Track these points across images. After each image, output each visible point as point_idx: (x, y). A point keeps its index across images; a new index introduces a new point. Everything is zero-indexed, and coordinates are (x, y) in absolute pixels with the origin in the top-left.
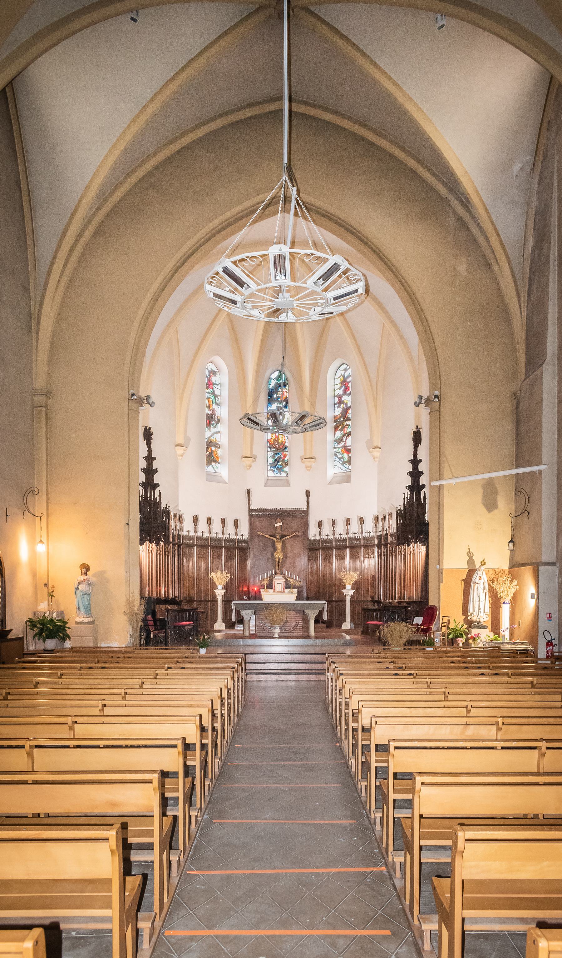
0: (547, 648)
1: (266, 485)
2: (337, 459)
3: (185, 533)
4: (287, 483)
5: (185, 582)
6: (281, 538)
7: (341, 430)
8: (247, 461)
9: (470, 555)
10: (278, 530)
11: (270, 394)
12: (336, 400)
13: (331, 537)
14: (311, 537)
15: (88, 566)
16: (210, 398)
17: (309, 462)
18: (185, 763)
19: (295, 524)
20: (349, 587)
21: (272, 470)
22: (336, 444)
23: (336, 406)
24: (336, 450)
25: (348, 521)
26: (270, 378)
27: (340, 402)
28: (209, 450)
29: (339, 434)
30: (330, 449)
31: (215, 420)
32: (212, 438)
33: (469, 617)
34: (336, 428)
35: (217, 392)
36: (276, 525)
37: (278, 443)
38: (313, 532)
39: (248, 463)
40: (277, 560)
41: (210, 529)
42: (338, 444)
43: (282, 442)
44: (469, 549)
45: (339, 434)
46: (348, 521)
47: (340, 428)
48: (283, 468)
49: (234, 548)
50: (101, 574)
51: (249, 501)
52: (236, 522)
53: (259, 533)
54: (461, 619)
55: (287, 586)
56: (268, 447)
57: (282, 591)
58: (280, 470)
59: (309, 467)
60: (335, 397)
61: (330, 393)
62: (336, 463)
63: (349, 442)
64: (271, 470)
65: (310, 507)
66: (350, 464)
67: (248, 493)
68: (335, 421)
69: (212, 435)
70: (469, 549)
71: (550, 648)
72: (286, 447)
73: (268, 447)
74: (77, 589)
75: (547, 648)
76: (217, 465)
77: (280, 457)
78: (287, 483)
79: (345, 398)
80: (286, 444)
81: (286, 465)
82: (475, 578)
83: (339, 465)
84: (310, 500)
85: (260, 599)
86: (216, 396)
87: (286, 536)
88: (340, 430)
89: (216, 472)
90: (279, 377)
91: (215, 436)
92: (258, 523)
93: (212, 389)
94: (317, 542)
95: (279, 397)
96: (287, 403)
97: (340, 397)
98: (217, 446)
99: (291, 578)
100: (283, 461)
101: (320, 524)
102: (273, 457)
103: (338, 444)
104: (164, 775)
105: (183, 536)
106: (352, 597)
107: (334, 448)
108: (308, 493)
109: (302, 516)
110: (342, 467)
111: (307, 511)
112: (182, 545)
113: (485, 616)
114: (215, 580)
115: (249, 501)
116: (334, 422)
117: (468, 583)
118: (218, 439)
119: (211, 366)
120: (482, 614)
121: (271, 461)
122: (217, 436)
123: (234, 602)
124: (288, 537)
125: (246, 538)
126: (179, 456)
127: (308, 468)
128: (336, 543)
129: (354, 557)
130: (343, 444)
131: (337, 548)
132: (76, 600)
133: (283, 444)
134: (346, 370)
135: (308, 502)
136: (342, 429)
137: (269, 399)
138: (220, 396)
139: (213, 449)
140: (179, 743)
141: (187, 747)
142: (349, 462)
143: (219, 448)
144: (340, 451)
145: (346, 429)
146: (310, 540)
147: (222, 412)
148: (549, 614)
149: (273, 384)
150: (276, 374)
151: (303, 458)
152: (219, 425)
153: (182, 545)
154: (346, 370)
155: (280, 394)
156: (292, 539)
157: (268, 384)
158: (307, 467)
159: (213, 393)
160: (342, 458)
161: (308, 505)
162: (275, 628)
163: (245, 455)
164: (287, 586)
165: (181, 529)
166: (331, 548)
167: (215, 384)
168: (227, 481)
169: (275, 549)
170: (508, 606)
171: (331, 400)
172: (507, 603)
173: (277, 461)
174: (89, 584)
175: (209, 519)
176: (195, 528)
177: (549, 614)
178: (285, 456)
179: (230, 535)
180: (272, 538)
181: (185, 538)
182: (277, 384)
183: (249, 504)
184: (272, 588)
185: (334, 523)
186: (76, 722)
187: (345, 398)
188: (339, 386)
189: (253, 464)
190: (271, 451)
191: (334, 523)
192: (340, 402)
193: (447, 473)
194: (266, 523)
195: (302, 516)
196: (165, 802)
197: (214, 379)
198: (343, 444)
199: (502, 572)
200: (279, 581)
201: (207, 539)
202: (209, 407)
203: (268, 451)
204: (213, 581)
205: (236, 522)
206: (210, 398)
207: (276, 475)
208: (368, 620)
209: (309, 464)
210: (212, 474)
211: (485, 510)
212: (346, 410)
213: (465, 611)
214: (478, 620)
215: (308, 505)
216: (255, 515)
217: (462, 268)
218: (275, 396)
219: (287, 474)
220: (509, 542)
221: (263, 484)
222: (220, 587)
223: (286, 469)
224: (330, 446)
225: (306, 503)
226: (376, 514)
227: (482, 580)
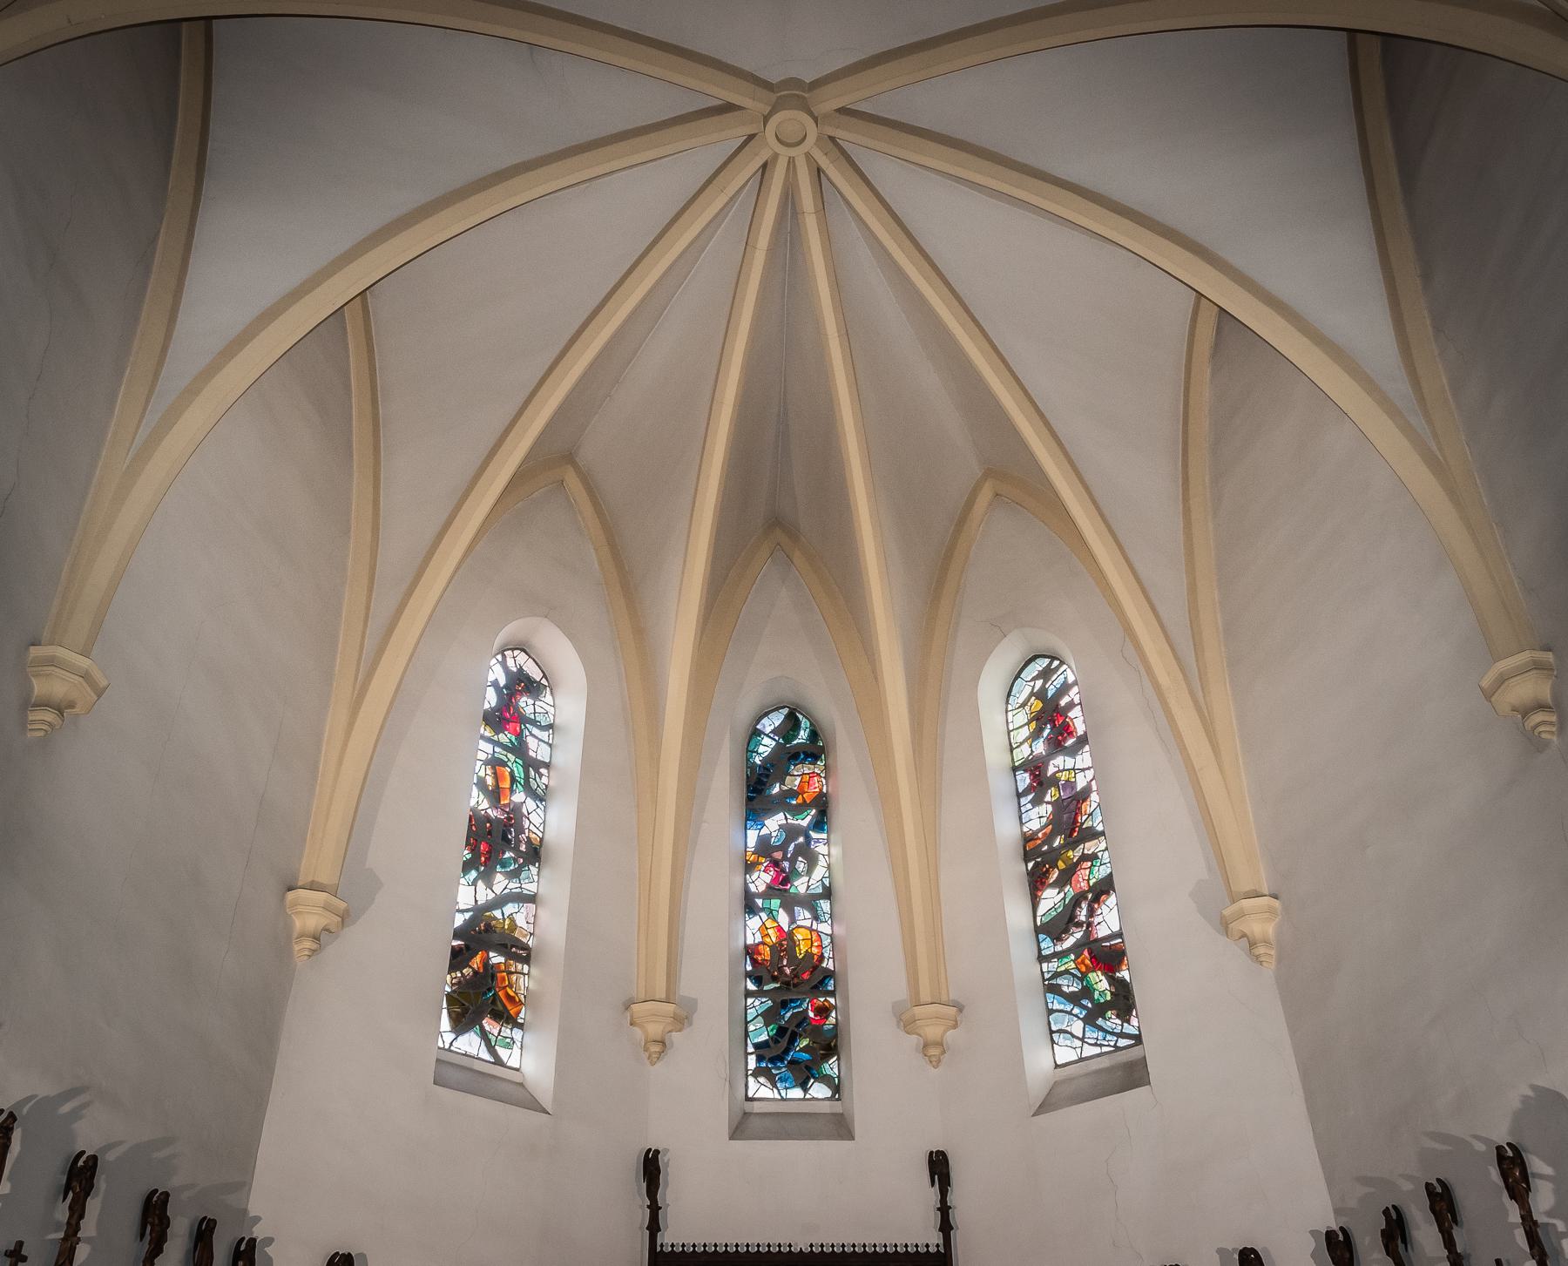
4: (840, 1127)
12: (1024, 779)
16: (504, 764)
22: (1048, 946)
26: (756, 733)
28: (476, 962)
29: (1051, 899)
30: (1024, 968)
31: (516, 850)
32: (497, 913)
34: (1036, 882)
35: (537, 749)
42: (1057, 938)
43: (808, 955)
45: (1051, 899)
47: (1055, 875)
51: (654, 1209)
56: (748, 975)
58: (804, 1074)
60: (1015, 769)
61: (995, 756)
62: (1058, 1022)
63: (1108, 920)
64: (757, 1073)
65: (957, 1237)
66: (1125, 1015)
69: (500, 902)
72: (829, 974)
73: (748, 975)
78: (840, 1127)
80: (828, 964)
83: (1077, 1027)
84: (952, 1199)
86: (531, 764)
88: (1056, 884)
89: (498, 1062)
91: (510, 908)
93: (519, 735)
95: (792, 794)
97: (1035, 767)
98: (518, 951)
102: (768, 1016)
103: (1057, 938)
107: (1042, 959)
108: (939, 1166)
110: (1092, 1034)
115: (654, 1209)
116: (1026, 862)
118: (520, 920)
121: (761, 1033)
134: (1046, 674)
135: (944, 1209)
138: (547, 766)
139: (496, 959)
142: (1123, 1001)
143: (526, 960)
145: (1082, 874)
147: (552, 822)
149: (766, 746)
150: (777, 719)
154: (1046, 674)
155: (794, 782)
157: (750, 751)
159: (519, 749)
160: (1087, 991)
161: (946, 1227)
167: (534, 723)
173: (785, 1036)
178: (823, 1011)
183: (654, 1227)
187: (1059, 762)
188: (1025, 732)
197: (525, 704)
202: (495, 795)
203: (748, 994)
206: (504, 764)
210: (477, 1066)
215: (946, 1227)
223: (831, 1067)
224: (1021, 949)
225: (934, 1219)
226: (1329, 1221)
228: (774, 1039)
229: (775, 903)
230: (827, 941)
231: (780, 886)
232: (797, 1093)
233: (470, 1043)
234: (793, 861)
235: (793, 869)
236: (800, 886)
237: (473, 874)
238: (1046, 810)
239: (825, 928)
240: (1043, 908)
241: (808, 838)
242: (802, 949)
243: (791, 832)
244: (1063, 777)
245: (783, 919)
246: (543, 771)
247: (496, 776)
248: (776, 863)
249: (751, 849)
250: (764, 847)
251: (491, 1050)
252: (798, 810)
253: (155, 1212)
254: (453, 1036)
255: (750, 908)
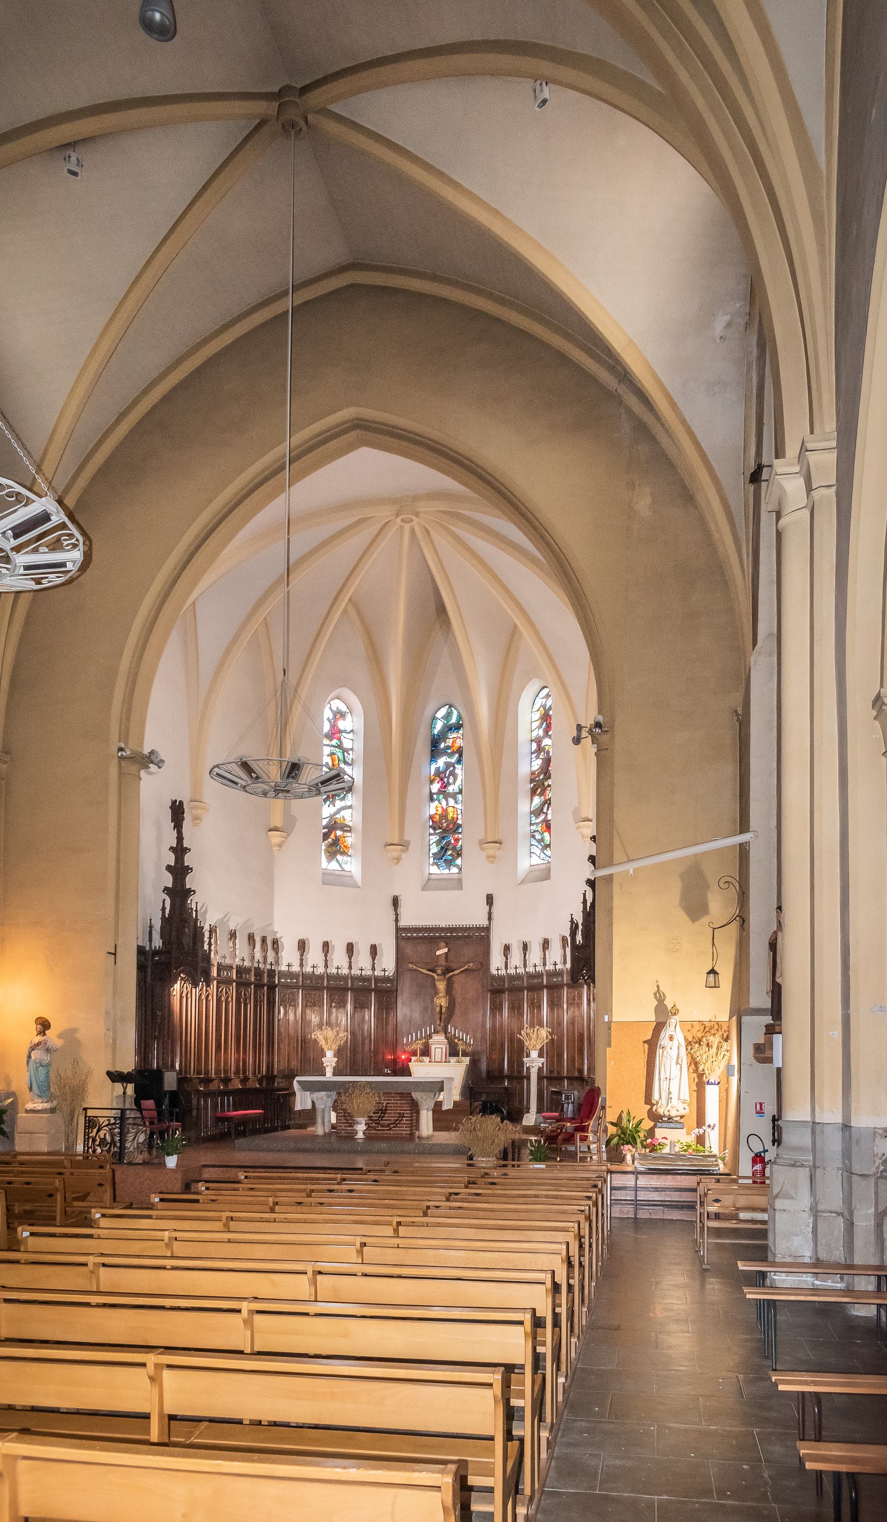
0: (753, 1166)
1: (424, 888)
2: (534, 842)
3: (284, 968)
5: (282, 1046)
6: (444, 974)
7: (541, 795)
8: (394, 851)
9: (660, 998)
10: (442, 962)
11: (435, 742)
12: (534, 746)
13: (521, 971)
14: (494, 972)
15: (47, 1021)
17: (492, 849)
18: (534, 1349)
19: (468, 952)
20: (534, 1054)
21: (436, 864)
22: (533, 818)
23: (534, 756)
24: (534, 828)
25: (546, 944)
27: (540, 749)
28: (332, 836)
29: (537, 800)
33: (654, 1108)
34: (533, 792)
35: (347, 744)
36: (438, 953)
37: (447, 820)
38: (496, 963)
39: (395, 854)
40: (438, 1009)
41: (326, 961)
42: (537, 817)
43: (453, 818)
44: (658, 987)
45: (537, 800)
46: (546, 944)
48: (454, 860)
49: (521, 990)
50: (69, 1035)
51: (397, 915)
52: (374, 950)
53: (411, 966)
54: (640, 1111)
55: (453, 1052)
56: (431, 827)
57: (444, 1059)
58: (449, 863)
59: (491, 857)
64: (434, 864)
65: (494, 923)
67: (396, 902)
68: (532, 781)
69: (338, 811)
70: (658, 987)
71: (758, 1167)
72: (460, 826)
73: (431, 827)
74: (29, 1057)
75: (753, 1166)
76: (345, 858)
77: (449, 843)
78: (458, 884)
79: (546, 742)
80: (459, 822)
81: (459, 855)
82: (664, 1040)
83: (537, 851)
84: (494, 910)
85: (409, 1074)
86: (345, 751)
87: (453, 971)
89: (343, 870)
90: (448, 715)
91: (343, 813)
92: (409, 950)
93: (339, 739)
94: (501, 978)
95: (448, 747)
96: (461, 755)
97: (539, 741)
99: (459, 1040)
100: (454, 849)
101: (507, 948)
102: (438, 843)
103: (537, 817)
104: (510, 1369)
105: (279, 972)
106: (540, 1070)
108: (490, 900)
109: (477, 939)
110: (542, 855)
111: (487, 929)
112: (276, 986)
113: (680, 1106)
114: (322, 1043)
115: (397, 915)
117: (652, 1044)
119: (337, 704)
120: (675, 1101)
121: (434, 849)
122: (346, 814)
123: (297, 1078)
124: (457, 972)
125: (391, 974)
126: (275, 845)
127: (491, 858)
128: (510, 981)
129: (554, 1004)
130: (542, 817)
131: (531, 989)
132: (28, 1074)
133: (454, 821)
135: (490, 914)
136: (542, 794)
137: (432, 751)
138: (352, 749)
139: (339, 833)
140: (527, 1318)
141: (538, 1323)
143: (350, 831)
144: (539, 829)
146: (493, 977)
148: (761, 1104)
149: (439, 726)
150: (443, 712)
151: (483, 843)
152: (350, 795)
153: (276, 986)
155: (449, 742)
156: (464, 975)
157: (432, 727)
158: (488, 857)
159: (340, 746)
160: (542, 840)
161: (490, 919)
162: (358, 1123)
163: (390, 842)
164: (453, 1052)
165: (277, 962)
166: (521, 990)
167: (345, 731)
168: (359, 882)
169: (436, 992)
170: (716, 1088)
171: (525, 747)
172: (712, 1084)
173: (444, 849)
174: (48, 1050)
175: (326, 946)
176: (302, 960)
177: (761, 1104)
178: (457, 840)
179: (362, 970)
180: (431, 973)
181: (282, 974)
182: (445, 726)
183: (397, 920)
184: (428, 1056)
185: (525, 947)
186: (320, 1273)
187: (546, 742)
188: (538, 723)
189: (403, 855)
190: (435, 834)
191: (525, 947)
192: (540, 749)
193: (618, 855)
194: (422, 948)
195: (477, 939)
196: (511, 1415)
197: (341, 724)
198: (542, 817)
199: (716, 1027)
200: (439, 1044)
201: (321, 977)
203: (430, 834)
204: (318, 1043)
205: (374, 950)
207: (443, 872)
208: (229, 1110)
209: (491, 852)
210: (337, 873)
211: (684, 918)
212: (547, 761)
213: (648, 1099)
214: (667, 1114)
215: (490, 919)
216: (410, 939)
217: (644, 504)
218: (442, 746)
219: (460, 870)
220: (708, 973)
221: (420, 888)
222: (329, 1054)
223: (459, 861)
225: (487, 916)
227: (675, 1040)
228: (440, 852)
229: (441, 796)
230: (459, 812)
231: (443, 791)
232: (447, 871)
233: (333, 866)
234: (448, 778)
235: (448, 782)
236: (451, 789)
237: (328, 803)
238: (539, 762)
239: (459, 806)
240: (534, 803)
241: (454, 767)
242: (451, 815)
243: (448, 765)
244: (547, 748)
245: (444, 802)
246: (350, 752)
247: (333, 760)
248: (442, 779)
249: (432, 773)
250: (438, 773)
251: (340, 865)
252: (451, 755)
253: (251, 938)
254: (334, 709)
255: (432, 799)
